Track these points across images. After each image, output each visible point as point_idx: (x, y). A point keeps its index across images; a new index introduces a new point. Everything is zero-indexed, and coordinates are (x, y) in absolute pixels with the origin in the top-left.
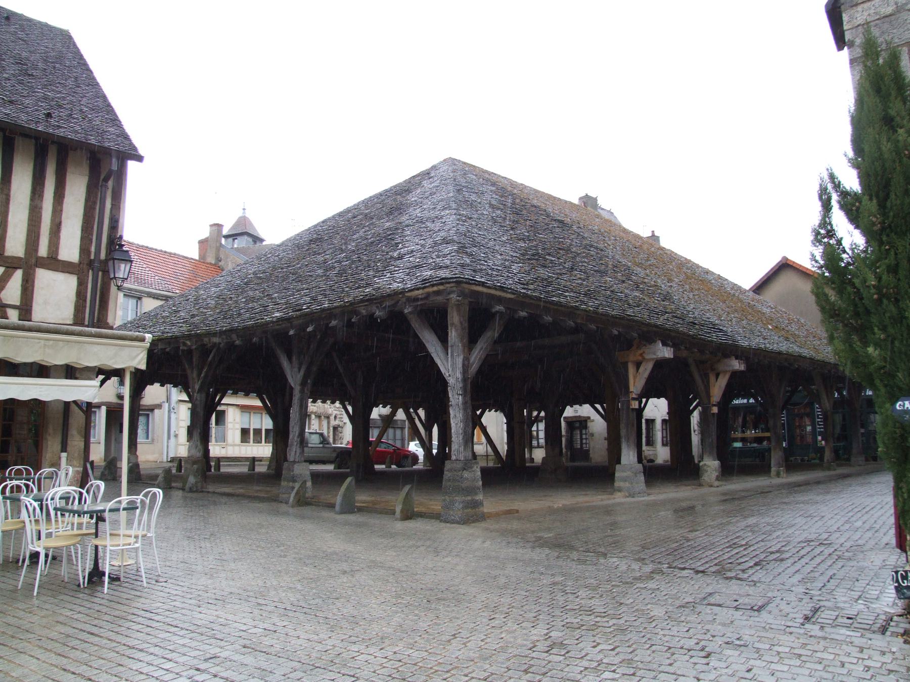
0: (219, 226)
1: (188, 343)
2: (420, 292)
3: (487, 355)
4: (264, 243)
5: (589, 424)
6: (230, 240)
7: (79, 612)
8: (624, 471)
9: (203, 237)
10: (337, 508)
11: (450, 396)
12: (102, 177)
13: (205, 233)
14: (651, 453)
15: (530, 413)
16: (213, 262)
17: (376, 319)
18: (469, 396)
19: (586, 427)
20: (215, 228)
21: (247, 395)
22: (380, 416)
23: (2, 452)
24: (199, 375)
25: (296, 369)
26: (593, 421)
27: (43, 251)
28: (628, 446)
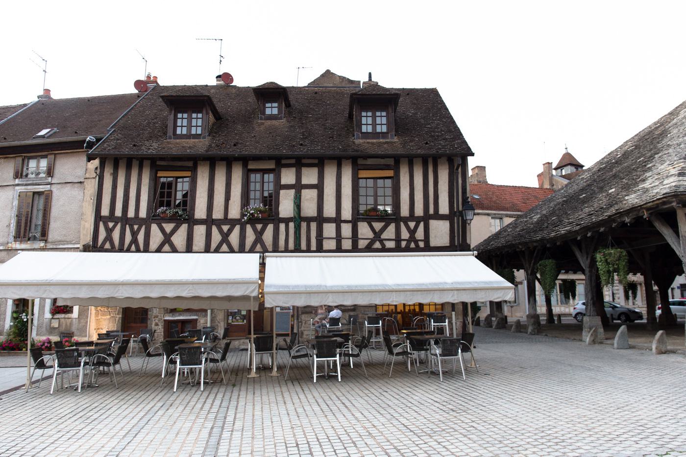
0: (550, 164)
1: (520, 247)
4: (584, 168)
6: (559, 170)
7: (475, 395)
9: (540, 172)
10: (616, 345)
12: (455, 168)
13: (541, 170)
16: (548, 187)
17: (627, 224)
21: (575, 273)
23: (685, 285)
24: (530, 265)
25: (585, 258)
27: (431, 211)
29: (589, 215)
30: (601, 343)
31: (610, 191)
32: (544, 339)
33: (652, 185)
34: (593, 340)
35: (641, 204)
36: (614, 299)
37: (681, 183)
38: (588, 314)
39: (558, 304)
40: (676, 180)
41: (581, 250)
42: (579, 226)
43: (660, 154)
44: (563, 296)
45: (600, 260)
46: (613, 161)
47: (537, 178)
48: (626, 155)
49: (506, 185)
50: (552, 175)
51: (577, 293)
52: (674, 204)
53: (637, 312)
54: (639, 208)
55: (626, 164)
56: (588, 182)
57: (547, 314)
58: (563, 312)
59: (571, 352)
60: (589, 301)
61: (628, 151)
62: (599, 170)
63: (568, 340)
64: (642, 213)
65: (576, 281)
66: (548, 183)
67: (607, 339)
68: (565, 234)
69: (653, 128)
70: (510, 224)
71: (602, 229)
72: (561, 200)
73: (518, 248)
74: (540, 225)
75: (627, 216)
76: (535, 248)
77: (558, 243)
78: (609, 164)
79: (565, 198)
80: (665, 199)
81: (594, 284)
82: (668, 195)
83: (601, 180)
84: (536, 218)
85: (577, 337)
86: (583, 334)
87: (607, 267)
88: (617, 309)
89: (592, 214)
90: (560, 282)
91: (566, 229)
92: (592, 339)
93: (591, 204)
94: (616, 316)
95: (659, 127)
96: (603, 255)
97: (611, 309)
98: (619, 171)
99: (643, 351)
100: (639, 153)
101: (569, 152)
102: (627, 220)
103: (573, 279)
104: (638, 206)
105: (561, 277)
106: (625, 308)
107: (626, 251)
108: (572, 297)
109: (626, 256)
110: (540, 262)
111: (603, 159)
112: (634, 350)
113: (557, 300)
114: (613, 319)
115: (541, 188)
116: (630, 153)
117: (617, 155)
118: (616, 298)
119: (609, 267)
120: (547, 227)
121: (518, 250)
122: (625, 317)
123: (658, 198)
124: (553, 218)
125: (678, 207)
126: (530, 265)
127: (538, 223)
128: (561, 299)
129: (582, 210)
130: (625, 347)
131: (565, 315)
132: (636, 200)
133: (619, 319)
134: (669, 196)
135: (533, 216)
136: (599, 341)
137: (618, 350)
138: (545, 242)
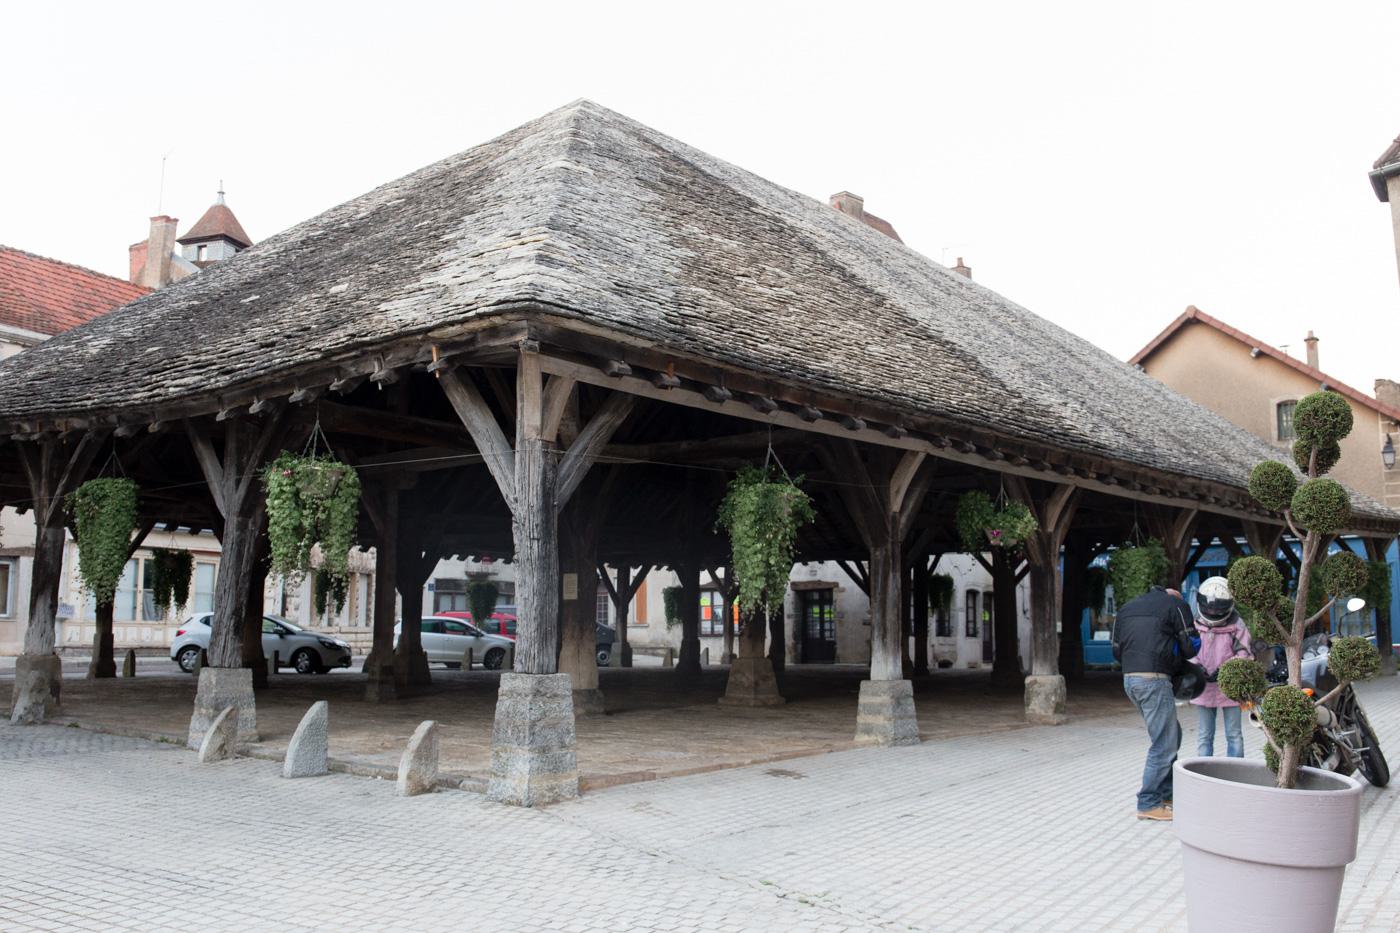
1: (27, 427)
2: (456, 329)
3: (595, 466)
5: (836, 595)
6: (194, 247)
8: (875, 694)
9: (139, 240)
10: (288, 765)
11: (516, 541)
13: (142, 233)
14: (946, 649)
15: (623, 576)
17: (375, 384)
18: (554, 543)
19: (830, 602)
20: (162, 223)
21: (194, 532)
22: (467, 573)
24: (52, 492)
25: (231, 483)
26: (843, 590)
28: (884, 644)
29: (262, 346)
30: (245, 754)
31: (334, 290)
32: (61, 743)
33: (460, 280)
34: (222, 747)
35: (428, 325)
36: (284, 609)
37: (546, 280)
38: (216, 662)
39: (134, 618)
40: (531, 271)
41: (221, 456)
42: (227, 377)
43: (477, 215)
44: (152, 596)
45: (277, 490)
46: (346, 225)
47: (128, 253)
48: (380, 215)
49: (28, 250)
50: (172, 255)
51: (192, 589)
52: (521, 338)
53: (339, 648)
54: (420, 337)
55: (379, 235)
56: (271, 269)
57: (94, 648)
58: (147, 642)
59: (141, 800)
60: (225, 620)
61: (388, 207)
62: (303, 242)
63: (142, 744)
64: (423, 355)
65: (194, 555)
66: (158, 274)
67: (261, 739)
68: (181, 397)
69: (452, 166)
70: (11, 359)
71: (297, 395)
72: (183, 305)
73: (19, 429)
74: (102, 370)
75: (379, 360)
76: (77, 435)
77: (153, 428)
78: (333, 231)
79: (195, 299)
80: (497, 320)
81: (245, 567)
82: (510, 306)
83: (310, 266)
84: (95, 346)
85: (172, 733)
86: (192, 724)
87: (296, 514)
88: (291, 638)
89: (273, 344)
90: (150, 555)
91: (185, 380)
92: (219, 741)
93: (272, 316)
94: (285, 657)
95: (468, 164)
96: (288, 476)
97: (276, 637)
98: (360, 247)
99: (367, 784)
100: (416, 213)
101: (229, 204)
102: (378, 371)
103: (187, 551)
104: (419, 332)
105: (151, 540)
106: (313, 636)
107: (357, 470)
108: (176, 600)
109: (354, 485)
110: (85, 484)
111: (317, 218)
112: (341, 777)
113: (135, 608)
114: (278, 664)
115: (135, 285)
116: (393, 211)
117: (357, 213)
118: (290, 607)
119: (302, 515)
120: (125, 373)
121: (15, 437)
122: (309, 659)
123: (478, 311)
124: (150, 350)
125: (531, 348)
126: (52, 492)
127: (102, 361)
128: (145, 604)
129: (243, 331)
130: (317, 771)
131: (150, 650)
132: (415, 314)
133: (293, 663)
134: (513, 311)
135: (89, 341)
136: (239, 745)
137: (296, 782)
138: (113, 418)
